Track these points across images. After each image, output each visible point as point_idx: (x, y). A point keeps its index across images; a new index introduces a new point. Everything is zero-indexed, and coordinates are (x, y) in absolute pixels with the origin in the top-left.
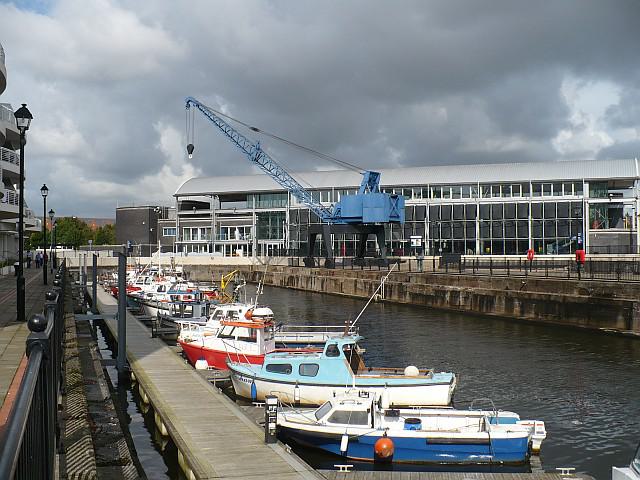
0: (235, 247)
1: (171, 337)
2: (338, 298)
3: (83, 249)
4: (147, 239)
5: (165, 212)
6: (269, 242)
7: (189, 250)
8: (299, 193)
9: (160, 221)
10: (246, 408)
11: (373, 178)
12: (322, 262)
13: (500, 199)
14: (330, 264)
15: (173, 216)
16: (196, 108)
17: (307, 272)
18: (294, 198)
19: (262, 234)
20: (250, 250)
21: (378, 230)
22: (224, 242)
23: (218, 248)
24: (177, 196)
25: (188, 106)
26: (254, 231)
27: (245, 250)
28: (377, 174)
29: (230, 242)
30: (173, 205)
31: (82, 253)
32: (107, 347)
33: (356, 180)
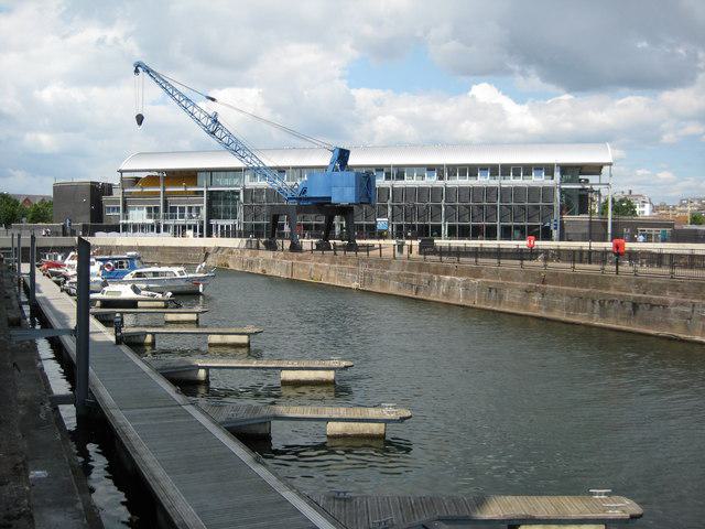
0: (184, 227)
1: (136, 340)
2: (564, 327)
3: (16, 227)
4: (89, 217)
5: (108, 189)
6: (221, 222)
7: (135, 231)
8: (257, 171)
9: (104, 198)
10: (268, 461)
11: (343, 155)
12: (287, 244)
13: (466, 182)
14: (295, 248)
15: (117, 194)
16: (145, 74)
17: (269, 255)
18: (247, 177)
19: (212, 214)
20: (201, 231)
21: (346, 211)
22: (170, 222)
23: (166, 228)
24: (121, 172)
25: (137, 71)
26: (204, 212)
27: (195, 231)
28: (348, 152)
29: (180, 221)
30: (116, 181)
31: (16, 232)
32: (53, 356)
33: (325, 159)
